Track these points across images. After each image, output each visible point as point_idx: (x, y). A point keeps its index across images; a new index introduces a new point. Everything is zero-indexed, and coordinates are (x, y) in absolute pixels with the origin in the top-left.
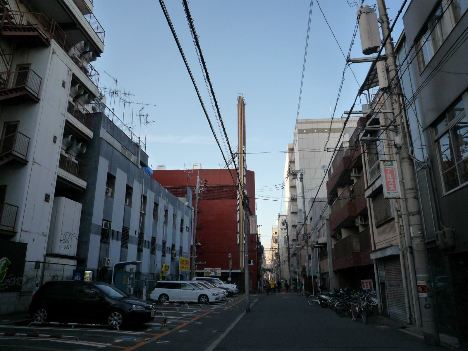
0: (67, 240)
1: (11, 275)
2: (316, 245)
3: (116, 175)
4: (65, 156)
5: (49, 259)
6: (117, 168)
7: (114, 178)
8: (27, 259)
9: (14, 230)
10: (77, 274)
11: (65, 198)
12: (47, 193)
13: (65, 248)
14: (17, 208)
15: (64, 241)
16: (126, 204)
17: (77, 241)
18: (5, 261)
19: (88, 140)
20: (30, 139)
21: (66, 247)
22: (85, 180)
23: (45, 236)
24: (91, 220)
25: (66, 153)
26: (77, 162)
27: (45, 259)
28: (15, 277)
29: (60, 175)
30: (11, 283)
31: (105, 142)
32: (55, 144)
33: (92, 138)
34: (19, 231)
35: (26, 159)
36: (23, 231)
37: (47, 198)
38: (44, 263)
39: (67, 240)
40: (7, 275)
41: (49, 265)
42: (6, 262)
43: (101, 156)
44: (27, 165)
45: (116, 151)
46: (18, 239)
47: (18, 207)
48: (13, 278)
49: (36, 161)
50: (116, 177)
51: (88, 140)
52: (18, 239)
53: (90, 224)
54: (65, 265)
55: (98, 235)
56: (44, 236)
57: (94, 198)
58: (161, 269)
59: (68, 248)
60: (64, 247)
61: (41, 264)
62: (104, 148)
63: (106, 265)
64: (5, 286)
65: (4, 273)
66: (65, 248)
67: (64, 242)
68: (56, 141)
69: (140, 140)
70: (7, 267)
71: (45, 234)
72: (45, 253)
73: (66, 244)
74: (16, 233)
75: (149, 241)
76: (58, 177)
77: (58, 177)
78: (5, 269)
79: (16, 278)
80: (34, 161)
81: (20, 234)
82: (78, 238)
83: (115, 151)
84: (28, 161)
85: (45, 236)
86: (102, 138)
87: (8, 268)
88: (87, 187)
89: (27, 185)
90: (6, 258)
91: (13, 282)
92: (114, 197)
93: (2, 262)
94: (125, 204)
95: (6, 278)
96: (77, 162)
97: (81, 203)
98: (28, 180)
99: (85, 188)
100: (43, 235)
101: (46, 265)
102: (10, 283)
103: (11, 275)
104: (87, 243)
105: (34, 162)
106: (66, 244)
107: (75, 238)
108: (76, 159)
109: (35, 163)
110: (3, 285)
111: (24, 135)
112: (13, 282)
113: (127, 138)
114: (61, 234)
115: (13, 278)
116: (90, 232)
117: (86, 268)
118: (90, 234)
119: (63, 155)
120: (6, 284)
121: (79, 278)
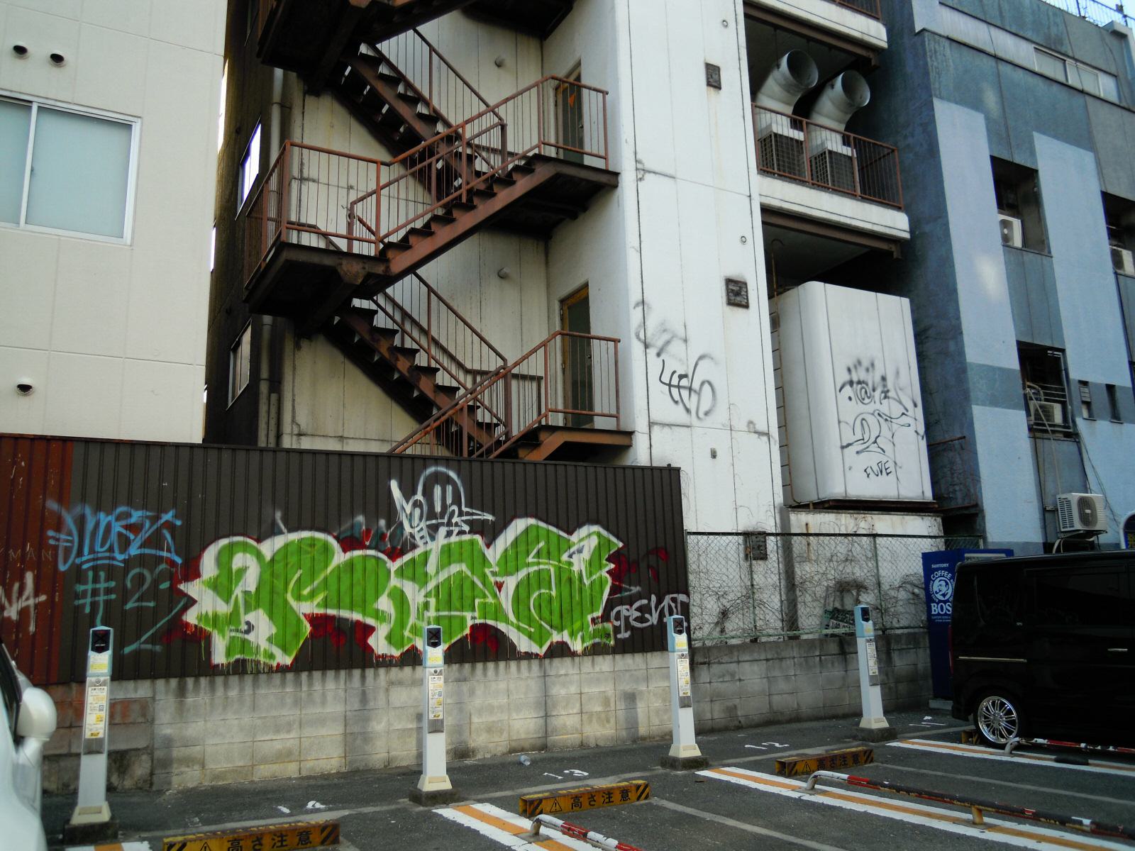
0: (875, 442)
1: (635, 589)
2: (541, 647)
3: (1036, 162)
4: (840, 154)
5: (799, 521)
6: (1036, 134)
7: (1030, 174)
8: (689, 525)
9: (618, 424)
10: (937, 570)
11: (822, 284)
12: (733, 273)
13: (872, 475)
14: (611, 343)
15: (860, 447)
16: (1119, 271)
17: (923, 444)
18: (594, 541)
19: (871, 55)
20: (605, 93)
21: (876, 468)
22: (899, 209)
23: (760, 434)
24: (961, 353)
25: (796, 124)
26: (847, 151)
27: (785, 522)
28: (653, 598)
29: (776, 203)
30: (641, 620)
31: (947, 43)
32: (721, 92)
33: (885, 45)
34: (640, 425)
35: (607, 164)
36: (656, 424)
37: (736, 293)
38: (786, 535)
39: (873, 439)
40: (614, 590)
41: (809, 544)
42: (599, 543)
43: (941, 98)
44: (619, 188)
45: (1009, 68)
46: (640, 455)
47: (616, 341)
48: (645, 602)
49: (648, 165)
50: (1037, 171)
51: (871, 55)
52: (640, 455)
53: (962, 369)
54: (879, 540)
55: (1020, 409)
56: (757, 435)
57: (952, 266)
58: (264, 761)
59: (883, 470)
60: (865, 471)
61: (771, 542)
62: (946, 64)
63: (1078, 526)
64: (617, 630)
65: (602, 583)
66: (872, 475)
67: (858, 452)
68: (719, 81)
69: (1125, 16)
70: (609, 560)
71: (762, 427)
72: (780, 499)
73: (872, 459)
74: (630, 434)
75: (1110, 388)
76: (766, 210)
77: (766, 210)
78: (600, 568)
79: (660, 601)
80: (639, 166)
81: (647, 437)
82: (922, 430)
83: (1004, 68)
84: (617, 171)
85: (760, 434)
86: (924, 30)
87: (612, 566)
88: (912, 231)
89: (632, 258)
90: (595, 528)
91: (647, 616)
92: (1050, 252)
93: (585, 543)
94: (1116, 273)
95: (610, 605)
96: (847, 151)
97: (901, 295)
98: (631, 239)
99: (907, 236)
100: (755, 432)
101: (798, 544)
102: (636, 620)
103: (635, 589)
104: (966, 444)
105: (642, 171)
106: (872, 459)
107: (912, 429)
108: (846, 142)
109: (649, 172)
110: (609, 626)
111: (595, 90)
112: (647, 616)
113: (1055, 14)
114: (839, 422)
115: (645, 602)
116: (965, 398)
117: (985, 539)
118: (971, 408)
119: (781, 136)
120: (617, 624)
121: (947, 584)
